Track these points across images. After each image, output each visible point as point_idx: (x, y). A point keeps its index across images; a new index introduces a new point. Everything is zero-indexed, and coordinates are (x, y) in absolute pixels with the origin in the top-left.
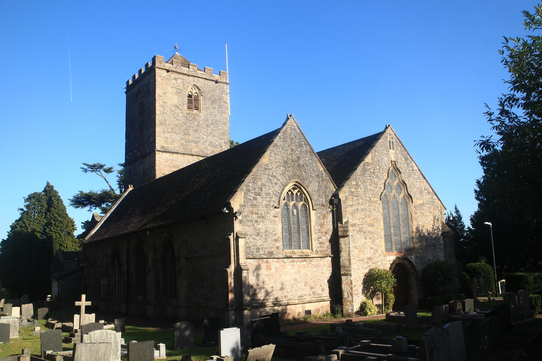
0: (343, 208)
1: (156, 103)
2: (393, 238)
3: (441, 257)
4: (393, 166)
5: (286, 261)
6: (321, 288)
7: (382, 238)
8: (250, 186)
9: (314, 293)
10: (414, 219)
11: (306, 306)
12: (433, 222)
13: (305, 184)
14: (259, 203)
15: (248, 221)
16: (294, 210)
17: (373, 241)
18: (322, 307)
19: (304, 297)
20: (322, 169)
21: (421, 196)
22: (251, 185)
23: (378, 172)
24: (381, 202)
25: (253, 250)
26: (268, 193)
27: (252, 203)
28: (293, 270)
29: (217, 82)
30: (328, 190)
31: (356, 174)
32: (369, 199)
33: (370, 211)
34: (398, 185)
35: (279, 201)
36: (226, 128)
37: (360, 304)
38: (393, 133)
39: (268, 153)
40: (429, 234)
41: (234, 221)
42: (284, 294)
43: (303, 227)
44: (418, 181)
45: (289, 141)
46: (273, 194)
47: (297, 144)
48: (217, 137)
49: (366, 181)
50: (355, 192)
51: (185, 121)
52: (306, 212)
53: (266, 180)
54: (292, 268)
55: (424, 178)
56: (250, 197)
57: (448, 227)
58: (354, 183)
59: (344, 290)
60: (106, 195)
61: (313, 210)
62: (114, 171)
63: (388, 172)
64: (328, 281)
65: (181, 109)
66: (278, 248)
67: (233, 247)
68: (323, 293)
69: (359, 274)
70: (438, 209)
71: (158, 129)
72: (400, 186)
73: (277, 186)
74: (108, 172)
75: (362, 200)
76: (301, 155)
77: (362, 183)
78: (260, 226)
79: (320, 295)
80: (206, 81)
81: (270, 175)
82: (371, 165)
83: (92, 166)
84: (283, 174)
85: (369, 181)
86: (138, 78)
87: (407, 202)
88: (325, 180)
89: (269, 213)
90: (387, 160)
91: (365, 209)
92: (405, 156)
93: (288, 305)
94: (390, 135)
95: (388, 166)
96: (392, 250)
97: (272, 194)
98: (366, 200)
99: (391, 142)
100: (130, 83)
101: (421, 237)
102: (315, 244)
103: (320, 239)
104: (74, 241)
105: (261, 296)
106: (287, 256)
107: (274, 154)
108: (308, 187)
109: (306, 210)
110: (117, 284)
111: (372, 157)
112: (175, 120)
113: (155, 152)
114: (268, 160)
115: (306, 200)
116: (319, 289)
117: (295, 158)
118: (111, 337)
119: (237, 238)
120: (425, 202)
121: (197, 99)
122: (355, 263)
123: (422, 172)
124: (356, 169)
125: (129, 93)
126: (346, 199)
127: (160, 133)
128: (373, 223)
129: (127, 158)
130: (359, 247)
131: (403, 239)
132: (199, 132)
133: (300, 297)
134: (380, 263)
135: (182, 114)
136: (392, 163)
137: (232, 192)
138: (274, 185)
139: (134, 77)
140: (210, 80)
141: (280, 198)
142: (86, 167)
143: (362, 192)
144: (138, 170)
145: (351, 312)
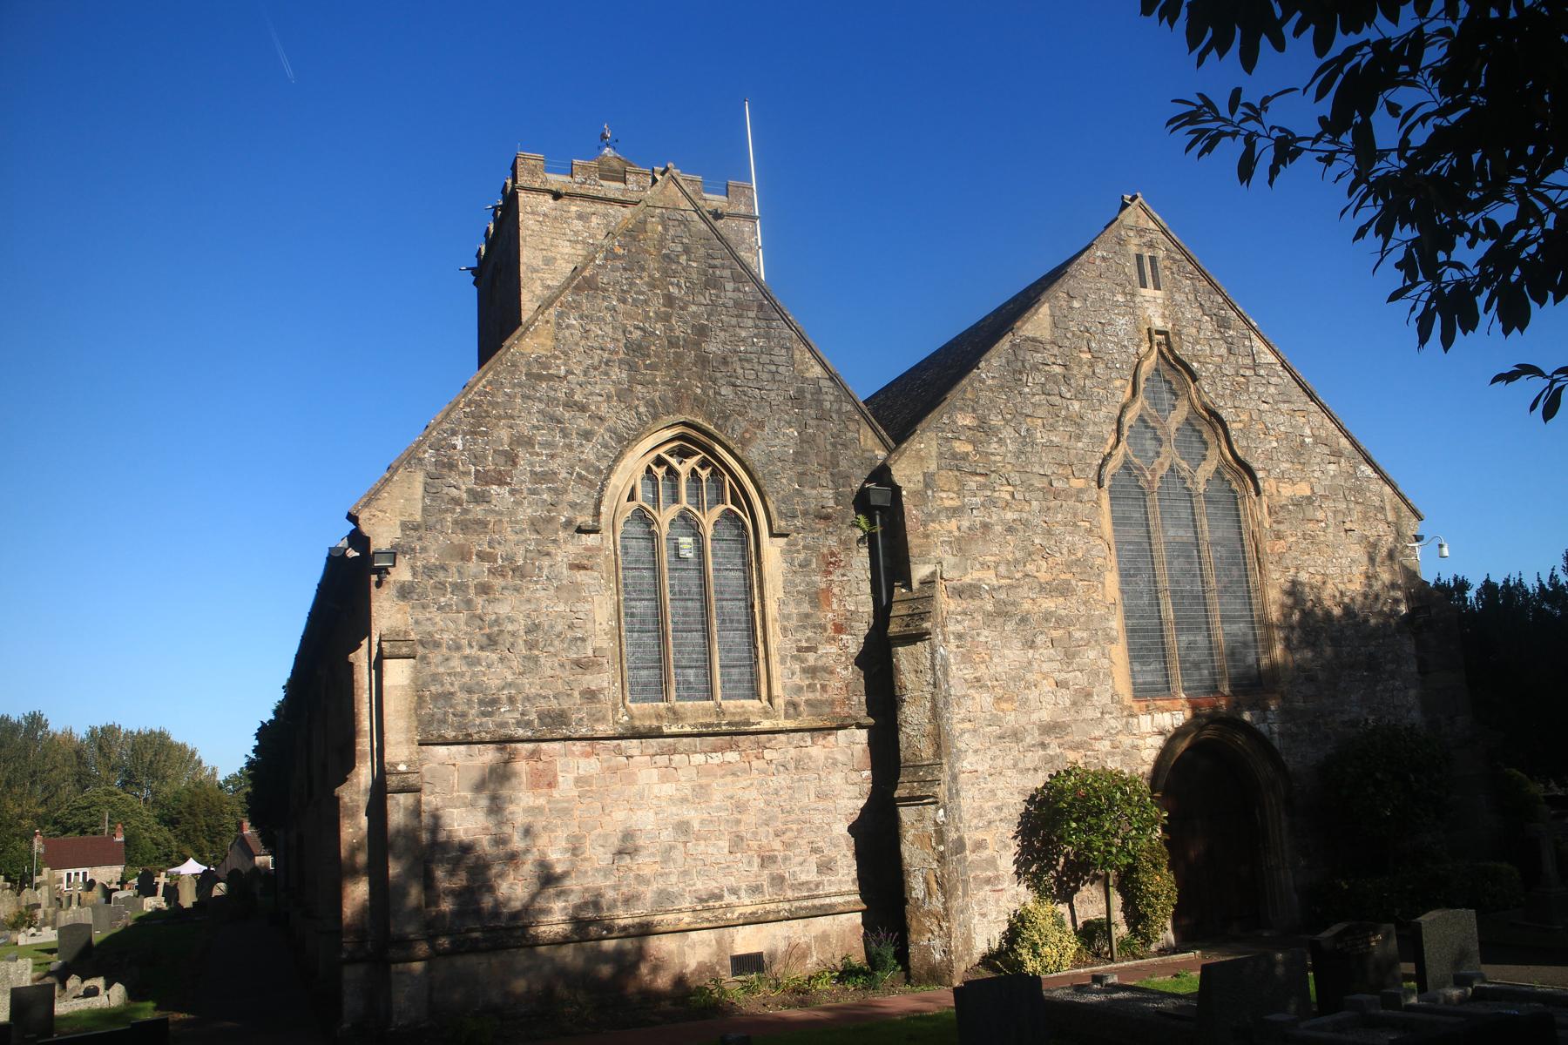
0: (910, 524)
2: (1175, 641)
5: (636, 752)
6: (814, 858)
7: (1112, 641)
9: (778, 881)
14: (500, 513)
16: (682, 540)
17: (1069, 656)
18: (824, 938)
19: (729, 899)
21: (1300, 467)
23: (1086, 377)
25: (465, 708)
26: (544, 474)
27: (461, 514)
28: (669, 789)
30: (850, 453)
31: (977, 384)
32: (1046, 485)
34: (1191, 425)
37: (1009, 921)
38: (1152, 225)
41: (374, 589)
42: (624, 889)
44: (1284, 407)
46: (571, 474)
47: (695, 276)
52: (745, 544)
53: (535, 422)
54: (664, 779)
56: (454, 492)
59: (911, 866)
61: (772, 535)
64: (850, 829)
66: (591, 695)
68: (825, 878)
69: (1000, 794)
70: (1383, 517)
72: (1199, 431)
75: (1010, 489)
77: (1007, 422)
78: (503, 609)
79: (810, 890)
81: (557, 399)
82: (1048, 347)
84: (623, 395)
85: (1040, 412)
87: (1233, 491)
88: (834, 416)
89: (548, 554)
91: (1026, 524)
92: (1215, 311)
94: (1141, 232)
96: (1169, 690)
98: (1030, 488)
102: (783, 677)
103: (811, 657)
106: (633, 728)
108: (744, 443)
109: (740, 532)
111: (1052, 315)
114: (550, 343)
116: (805, 861)
117: (680, 330)
119: (377, 666)
120: (1319, 491)
122: (976, 751)
126: (927, 486)
128: (1068, 582)
130: (995, 683)
133: (706, 901)
134: (1105, 746)
136: (1151, 341)
138: (575, 441)
143: (1005, 456)
145: (942, 961)
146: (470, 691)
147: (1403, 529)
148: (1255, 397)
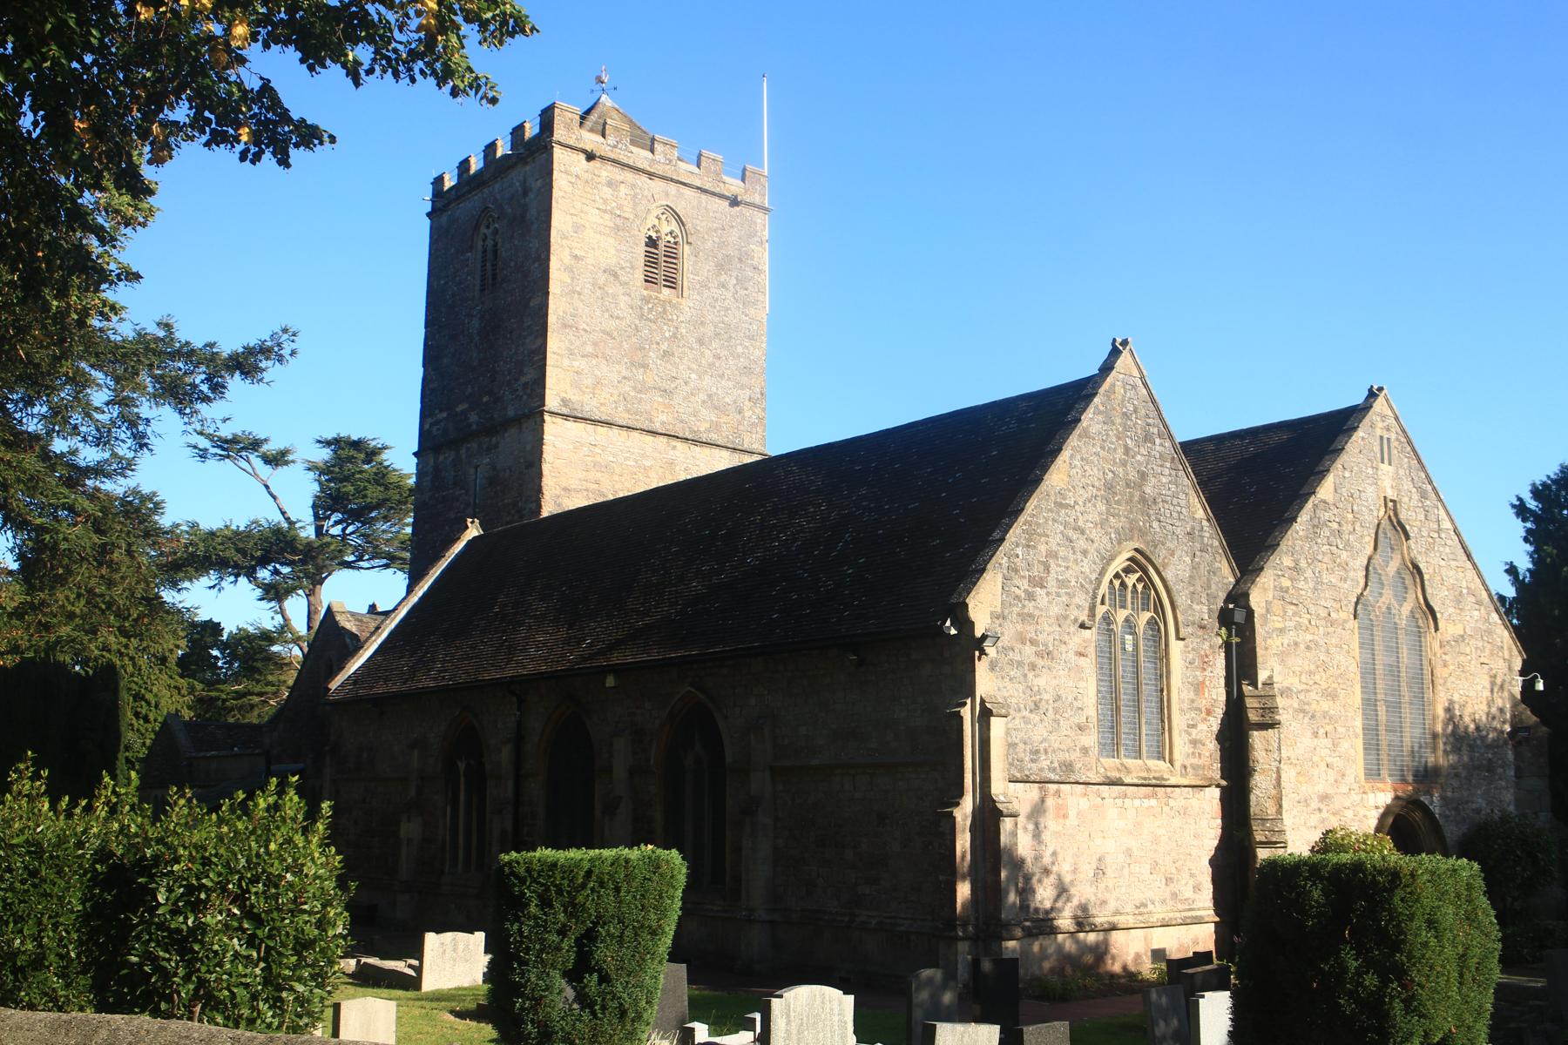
1: (552, 257)
2: (1384, 737)
3: (1508, 805)
4: (1389, 517)
5: (1105, 795)
6: (1191, 882)
8: (1017, 556)
9: (1174, 895)
10: (1438, 681)
11: (1154, 936)
12: (1489, 694)
13: (1159, 557)
14: (1041, 610)
15: (1011, 662)
19: (1151, 907)
20: (1200, 514)
22: (1020, 553)
24: (1356, 626)
29: (734, 202)
31: (1294, 535)
33: (1328, 652)
35: (1092, 609)
36: (757, 352)
38: (1390, 413)
39: (1065, 455)
40: (1478, 728)
43: (1148, 690)
44: (1453, 564)
45: (1118, 421)
47: (1139, 432)
48: (729, 379)
49: (1320, 558)
50: (1291, 591)
51: (637, 322)
55: (1469, 557)
56: (1018, 592)
57: (1532, 712)
58: (1287, 561)
60: (278, 539)
62: (293, 462)
63: (1377, 534)
65: (626, 284)
66: (1085, 750)
67: (970, 742)
68: (1197, 896)
71: (555, 343)
72: (1403, 579)
73: (1086, 561)
74: (277, 465)
75: (1308, 616)
76: (1149, 467)
77: (1309, 565)
80: (704, 197)
83: (226, 441)
84: (1102, 524)
85: (1326, 560)
86: (480, 173)
87: (1419, 627)
89: (1065, 643)
90: (1375, 495)
93: (1114, 928)
94: (1384, 418)
95: (1375, 513)
96: (1379, 775)
97: (1073, 583)
99: (1385, 441)
100: (449, 183)
101: (1460, 739)
103: (1194, 731)
104: (175, 687)
105: (1044, 895)
107: (1082, 459)
112: (606, 315)
113: (542, 415)
114: (1066, 479)
115: (1159, 608)
117: (1133, 475)
118: (832, 1010)
119: (985, 715)
121: (672, 255)
123: (1465, 539)
124: (1294, 519)
125: (444, 218)
127: (558, 354)
131: (1407, 740)
132: (677, 360)
135: (627, 298)
137: (969, 572)
139: (464, 165)
140: (714, 194)
141: (1094, 597)
142: (204, 443)
144: (472, 471)
146: (1025, 743)
147: (1513, 665)
148: (1438, 554)
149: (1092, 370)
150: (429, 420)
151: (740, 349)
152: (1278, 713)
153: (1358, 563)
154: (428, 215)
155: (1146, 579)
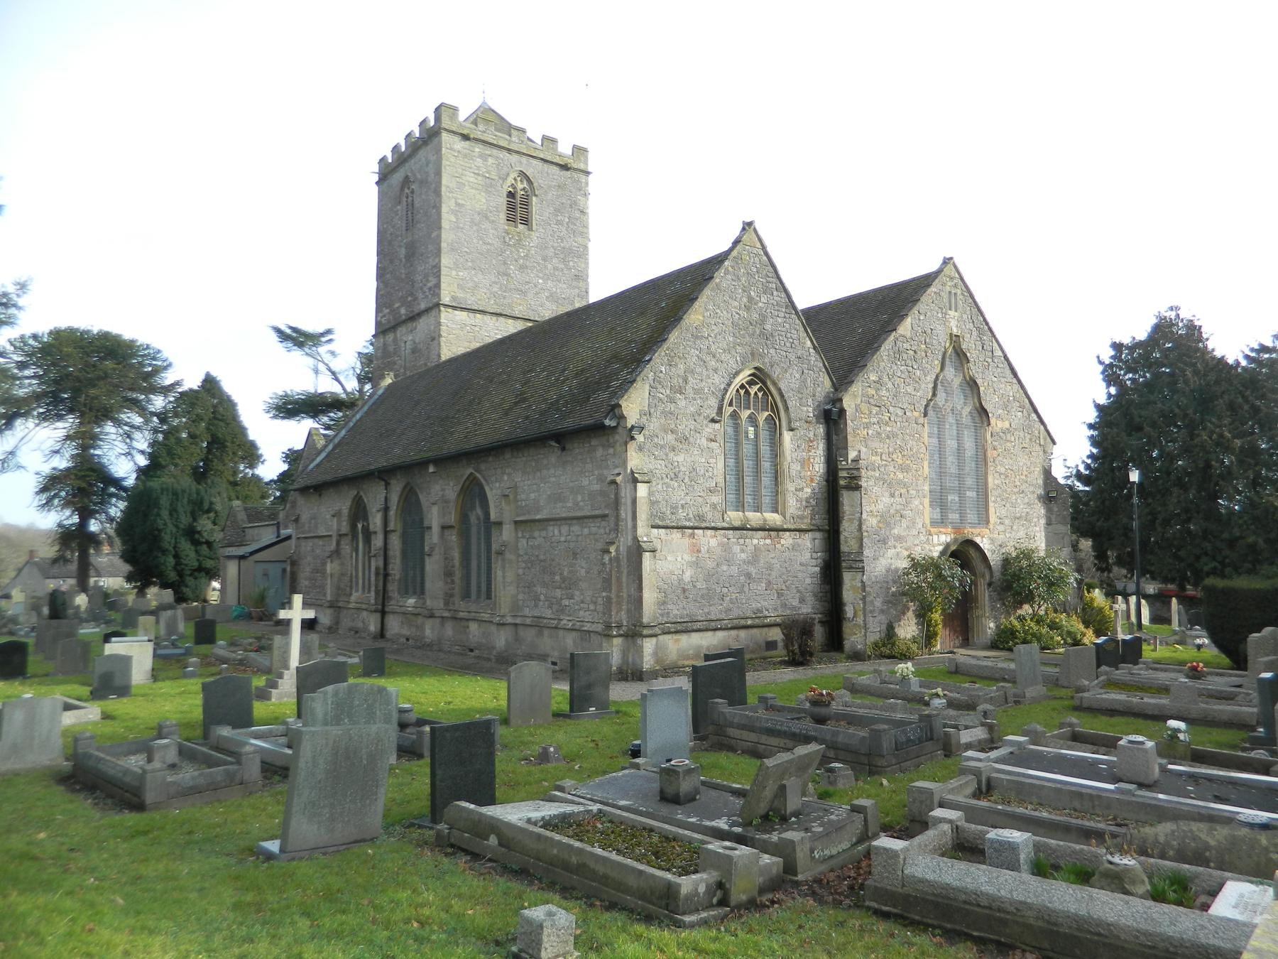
5: (731, 536)
8: (661, 372)
10: (990, 459)
13: (776, 373)
15: (656, 445)
22: (663, 370)
44: (1003, 380)
65: (493, 221)
94: (952, 278)
95: (943, 344)
110: (360, 574)
112: (481, 242)
115: (775, 408)
121: (526, 204)
125: (385, 184)
129: (379, 319)
140: (552, 163)
144: (403, 345)
149: (726, 246)
150: (380, 315)
151: (571, 264)
152: (861, 481)
153: (928, 378)
154: (377, 183)
155: (766, 391)
